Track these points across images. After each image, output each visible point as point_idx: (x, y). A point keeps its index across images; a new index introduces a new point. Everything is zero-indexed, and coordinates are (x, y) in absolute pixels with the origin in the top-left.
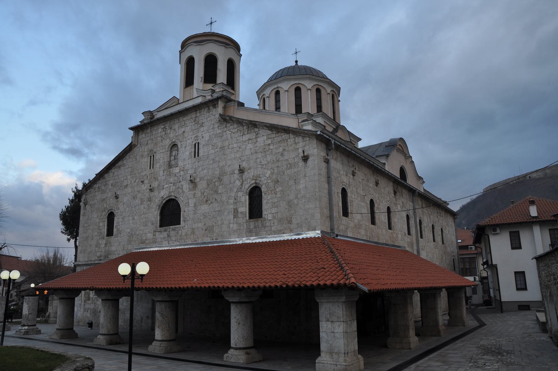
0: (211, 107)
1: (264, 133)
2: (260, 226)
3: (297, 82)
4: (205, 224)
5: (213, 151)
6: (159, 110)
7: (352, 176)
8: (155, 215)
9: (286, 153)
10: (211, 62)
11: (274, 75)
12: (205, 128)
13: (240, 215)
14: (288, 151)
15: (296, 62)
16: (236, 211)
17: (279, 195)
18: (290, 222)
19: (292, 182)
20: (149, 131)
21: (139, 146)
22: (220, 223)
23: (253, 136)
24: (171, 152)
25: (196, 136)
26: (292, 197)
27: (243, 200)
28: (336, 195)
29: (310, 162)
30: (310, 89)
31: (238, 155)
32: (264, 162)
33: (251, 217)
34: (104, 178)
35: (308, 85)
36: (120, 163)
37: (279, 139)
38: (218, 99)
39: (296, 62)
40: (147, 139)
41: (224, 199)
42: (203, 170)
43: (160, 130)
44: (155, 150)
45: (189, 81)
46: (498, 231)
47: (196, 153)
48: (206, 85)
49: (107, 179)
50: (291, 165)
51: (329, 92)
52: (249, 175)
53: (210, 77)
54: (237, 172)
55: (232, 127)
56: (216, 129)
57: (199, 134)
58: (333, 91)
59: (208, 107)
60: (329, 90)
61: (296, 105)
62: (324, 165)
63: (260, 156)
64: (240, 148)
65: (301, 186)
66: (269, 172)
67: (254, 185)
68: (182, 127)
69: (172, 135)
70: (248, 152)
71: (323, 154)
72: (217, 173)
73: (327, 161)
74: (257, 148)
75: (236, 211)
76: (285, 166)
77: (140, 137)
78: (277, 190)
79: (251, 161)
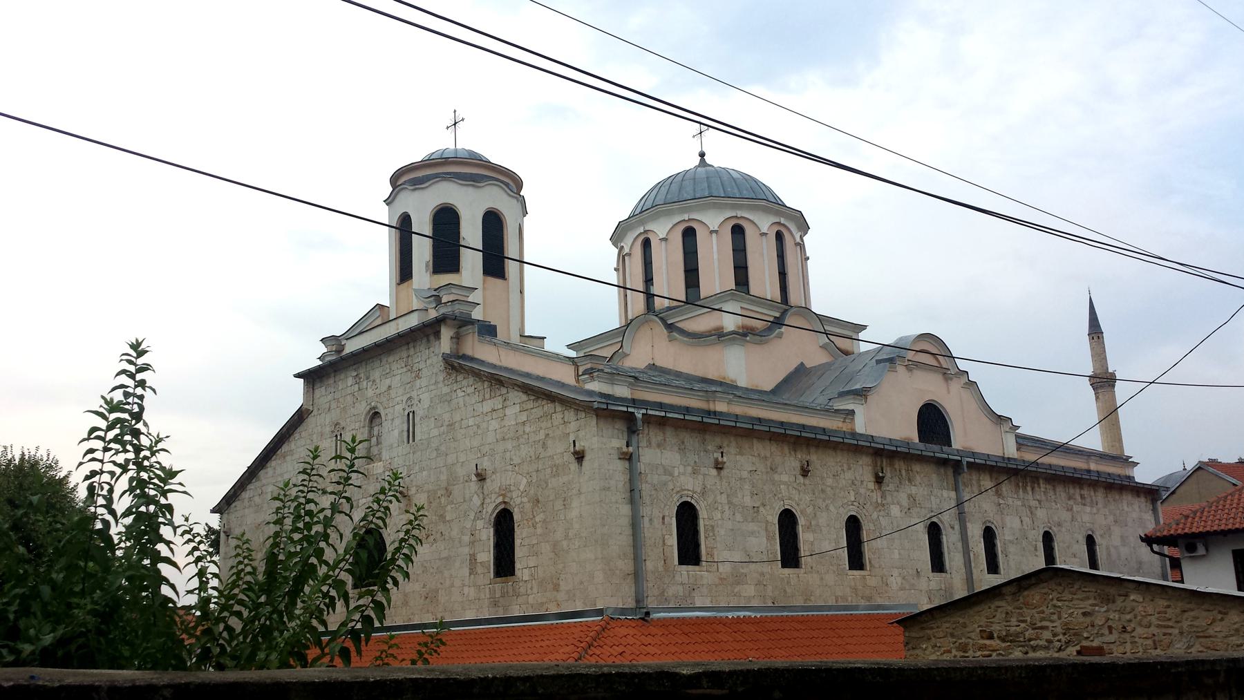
0: (432, 338)
1: (516, 397)
2: (510, 590)
3: (686, 217)
4: (424, 586)
5: (435, 432)
6: (358, 329)
7: (714, 472)
8: (587, 458)
9: (549, 443)
10: (446, 220)
11: (652, 190)
12: (423, 382)
13: (480, 570)
14: (553, 438)
15: (702, 155)
16: (473, 558)
17: (539, 531)
18: (556, 588)
19: (559, 505)
20: (331, 381)
21: (315, 412)
22: (448, 583)
23: (497, 403)
24: (371, 428)
25: (410, 398)
26: (559, 535)
27: (484, 537)
28: (657, 522)
29: (586, 463)
30: (716, 232)
31: (476, 443)
32: (517, 460)
33: (498, 574)
34: (259, 480)
35: (712, 220)
36: (285, 448)
37: (538, 412)
38: (440, 321)
39: (702, 155)
40: (330, 397)
41: (454, 533)
42: (422, 470)
43: (350, 381)
44: (343, 424)
45: (404, 271)
46: (1201, 550)
47: (410, 435)
48: (436, 277)
49: (264, 481)
50: (557, 466)
51: (764, 230)
52: (493, 484)
53: (446, 257)
54: (474, 478)
55: (465, 383)
56: (441, 385)
57: (414, 394)
58: (779, 223)
59: (427, 336)
60: (765, 223)
61: (686, 271)
62: (621, 466)
63: (510, 447)
64: (478, 427)
65: (574, 513)
66: (525, 481)
67: (502, 506)
68: (386, 375)
69: (370, 393)
70: (491, 438)
71: (618, 442)
72: (444, 477)
73: (628, 458)
74: (505, 430)
75: (473, 558)
76: (549, 471)
77: (318, 393)
78: (537, 519)
79: (497, 457)
